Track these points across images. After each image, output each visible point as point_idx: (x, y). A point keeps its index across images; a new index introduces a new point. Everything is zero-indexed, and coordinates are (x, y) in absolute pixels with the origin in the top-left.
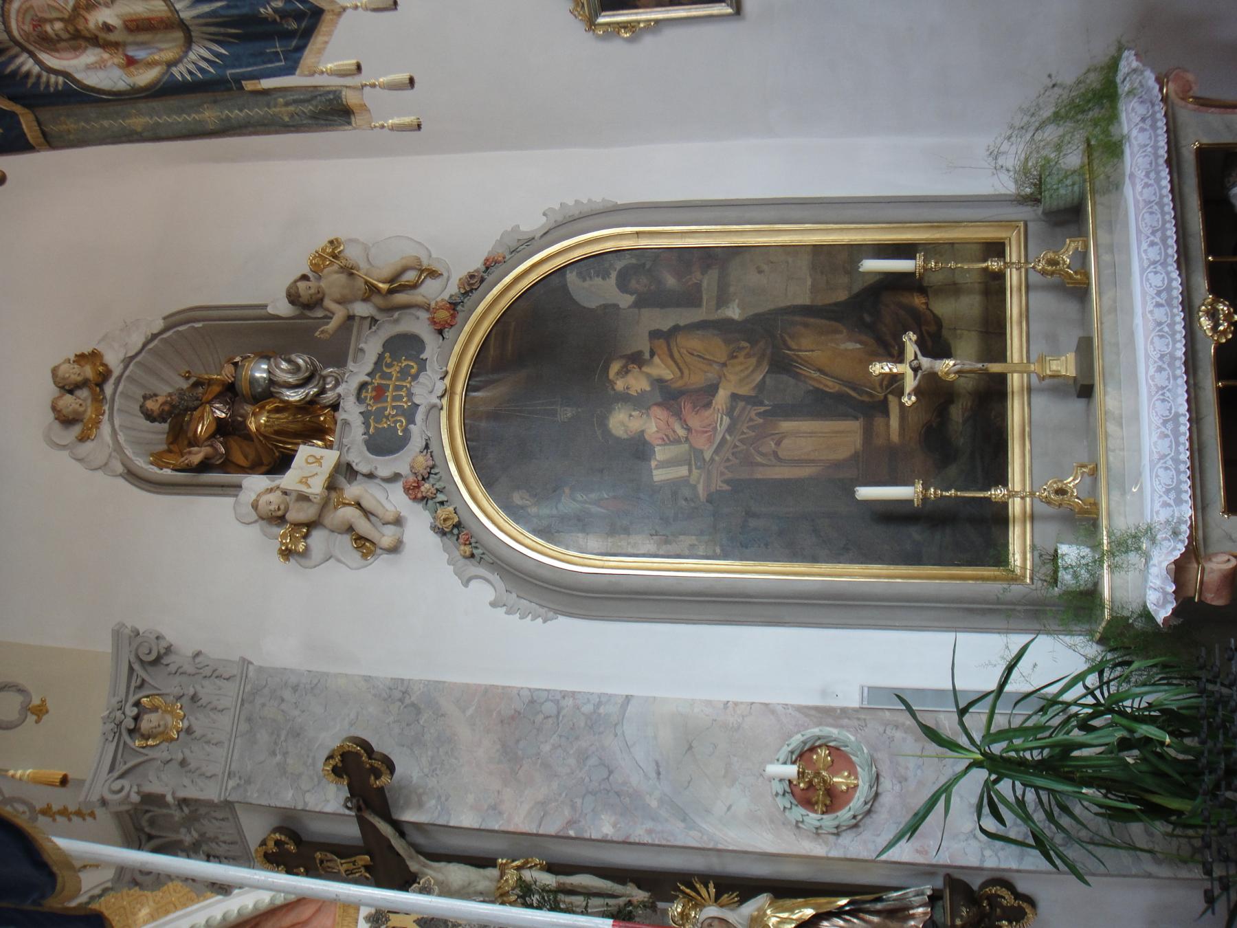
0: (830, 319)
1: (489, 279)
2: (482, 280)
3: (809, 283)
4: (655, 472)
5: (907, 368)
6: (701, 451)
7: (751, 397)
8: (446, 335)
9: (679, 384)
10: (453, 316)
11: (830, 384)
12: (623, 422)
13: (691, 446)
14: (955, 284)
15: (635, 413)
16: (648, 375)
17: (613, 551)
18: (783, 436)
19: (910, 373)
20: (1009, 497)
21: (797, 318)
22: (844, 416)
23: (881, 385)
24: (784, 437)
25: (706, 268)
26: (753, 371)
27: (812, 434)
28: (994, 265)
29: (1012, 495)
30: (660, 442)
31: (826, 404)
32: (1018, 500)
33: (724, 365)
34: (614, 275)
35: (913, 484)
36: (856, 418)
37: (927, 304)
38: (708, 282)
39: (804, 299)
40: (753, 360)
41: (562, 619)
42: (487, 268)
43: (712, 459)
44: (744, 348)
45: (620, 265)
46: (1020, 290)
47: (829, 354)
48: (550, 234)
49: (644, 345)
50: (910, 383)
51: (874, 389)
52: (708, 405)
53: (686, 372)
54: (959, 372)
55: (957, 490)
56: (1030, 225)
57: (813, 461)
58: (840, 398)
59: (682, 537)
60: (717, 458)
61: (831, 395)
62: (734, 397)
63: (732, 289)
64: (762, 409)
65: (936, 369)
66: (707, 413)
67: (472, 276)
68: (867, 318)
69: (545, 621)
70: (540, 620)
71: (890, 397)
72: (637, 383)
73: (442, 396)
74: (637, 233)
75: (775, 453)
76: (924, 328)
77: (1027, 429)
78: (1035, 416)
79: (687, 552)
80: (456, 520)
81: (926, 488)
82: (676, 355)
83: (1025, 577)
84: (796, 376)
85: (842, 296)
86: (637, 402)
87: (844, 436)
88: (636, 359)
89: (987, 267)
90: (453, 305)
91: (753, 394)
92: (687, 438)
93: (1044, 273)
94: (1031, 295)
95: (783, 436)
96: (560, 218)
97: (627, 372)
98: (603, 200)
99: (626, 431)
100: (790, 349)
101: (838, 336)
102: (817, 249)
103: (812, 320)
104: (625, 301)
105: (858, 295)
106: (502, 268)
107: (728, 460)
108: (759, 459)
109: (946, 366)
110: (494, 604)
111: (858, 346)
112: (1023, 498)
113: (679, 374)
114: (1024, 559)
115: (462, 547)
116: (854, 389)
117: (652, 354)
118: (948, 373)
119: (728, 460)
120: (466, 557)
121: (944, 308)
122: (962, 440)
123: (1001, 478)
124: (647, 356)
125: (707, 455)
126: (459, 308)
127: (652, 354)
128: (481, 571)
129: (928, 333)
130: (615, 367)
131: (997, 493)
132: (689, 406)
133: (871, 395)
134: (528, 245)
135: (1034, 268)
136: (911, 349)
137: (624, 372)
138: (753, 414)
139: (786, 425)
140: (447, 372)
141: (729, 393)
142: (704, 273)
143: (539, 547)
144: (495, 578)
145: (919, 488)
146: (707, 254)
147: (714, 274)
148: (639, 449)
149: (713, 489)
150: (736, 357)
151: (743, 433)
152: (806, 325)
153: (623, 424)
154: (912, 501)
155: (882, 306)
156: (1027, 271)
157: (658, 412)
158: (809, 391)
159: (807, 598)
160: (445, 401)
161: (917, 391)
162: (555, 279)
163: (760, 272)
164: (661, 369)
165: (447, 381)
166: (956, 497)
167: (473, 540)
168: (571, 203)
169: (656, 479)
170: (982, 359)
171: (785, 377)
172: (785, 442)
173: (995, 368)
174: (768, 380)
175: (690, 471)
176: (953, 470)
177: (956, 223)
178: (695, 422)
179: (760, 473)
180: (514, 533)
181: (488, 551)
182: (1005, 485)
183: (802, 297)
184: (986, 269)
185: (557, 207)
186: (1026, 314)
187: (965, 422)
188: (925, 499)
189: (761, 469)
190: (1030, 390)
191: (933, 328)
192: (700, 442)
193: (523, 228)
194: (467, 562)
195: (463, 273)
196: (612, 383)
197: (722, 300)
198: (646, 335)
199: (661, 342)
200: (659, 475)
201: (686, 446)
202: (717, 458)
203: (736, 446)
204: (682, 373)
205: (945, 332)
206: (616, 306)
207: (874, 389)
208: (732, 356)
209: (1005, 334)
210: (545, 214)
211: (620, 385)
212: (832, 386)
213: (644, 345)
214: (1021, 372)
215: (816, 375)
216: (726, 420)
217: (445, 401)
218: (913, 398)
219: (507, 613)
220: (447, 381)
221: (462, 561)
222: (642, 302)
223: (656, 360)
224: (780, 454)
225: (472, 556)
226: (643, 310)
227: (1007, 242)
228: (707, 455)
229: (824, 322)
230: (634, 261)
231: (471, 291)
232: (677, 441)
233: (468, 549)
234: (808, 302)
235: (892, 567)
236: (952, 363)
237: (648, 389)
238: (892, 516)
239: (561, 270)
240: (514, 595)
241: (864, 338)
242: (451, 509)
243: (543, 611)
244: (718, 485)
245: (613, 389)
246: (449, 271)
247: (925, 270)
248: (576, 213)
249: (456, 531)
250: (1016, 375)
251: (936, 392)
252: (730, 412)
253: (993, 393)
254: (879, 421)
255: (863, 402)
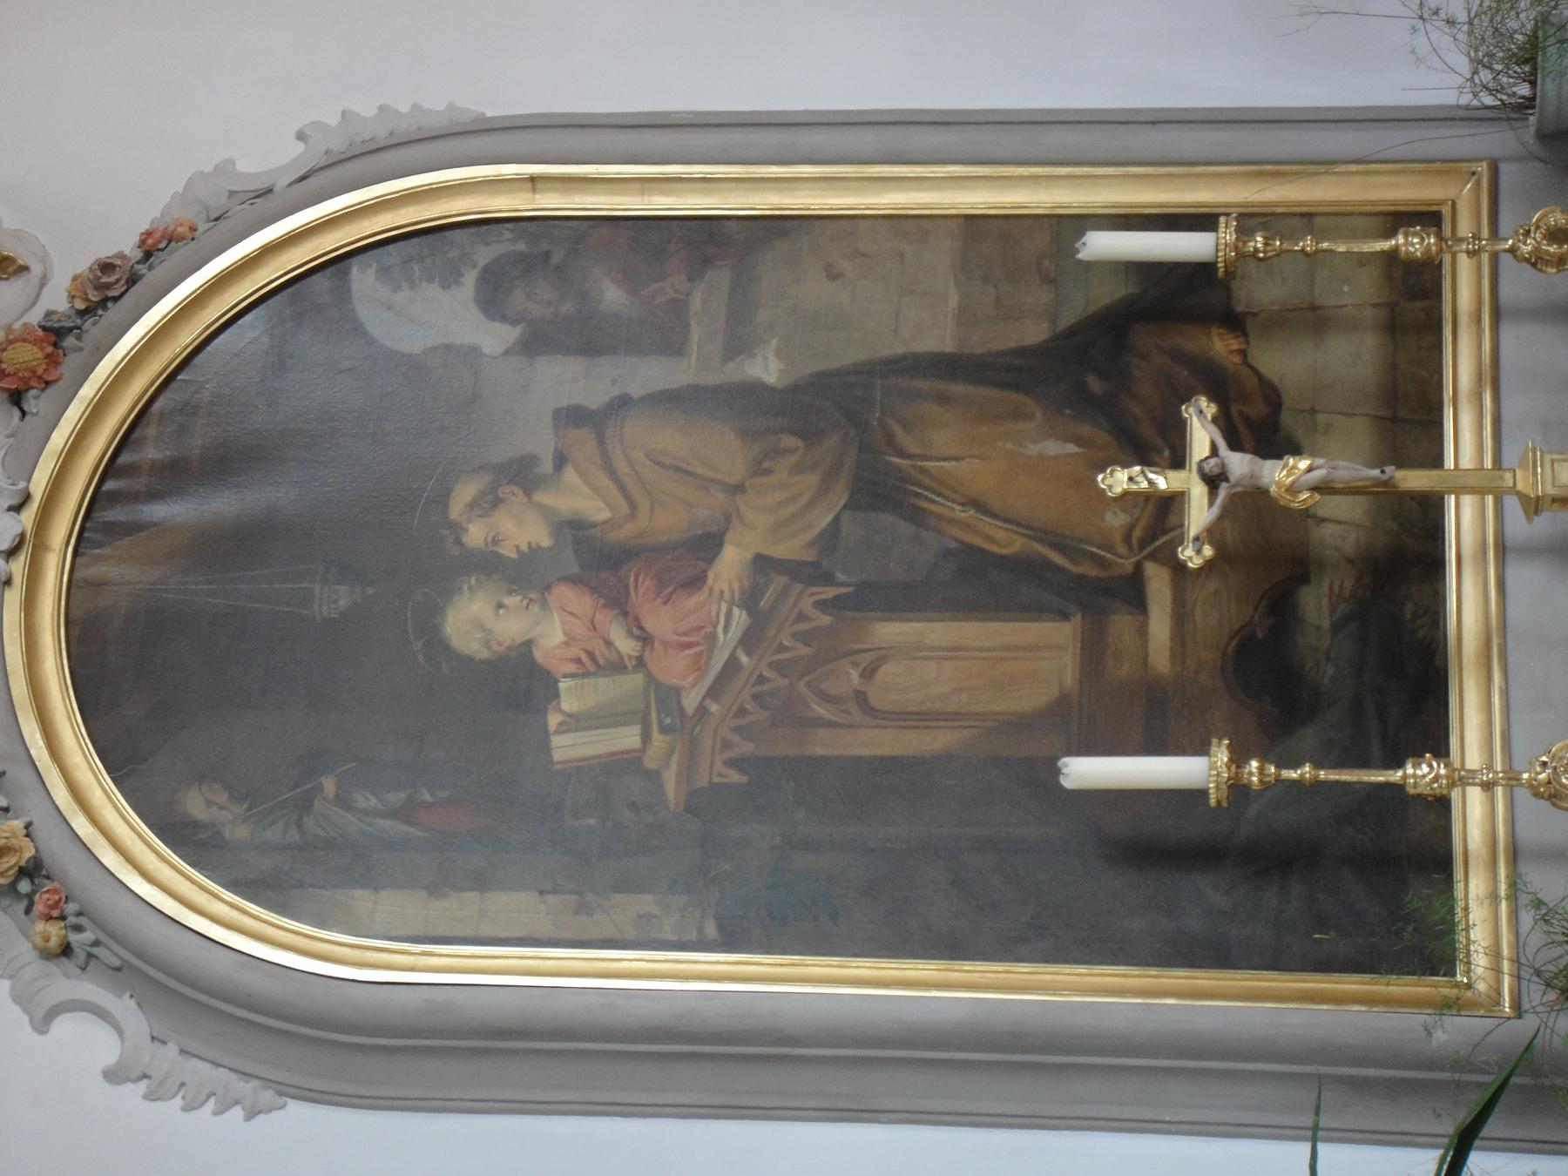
0: (1002, 385)
1: (151, 277)
2: (133, 280)
3: (953, 302)
4: (556, 741)
5: (1198, 476)
6: (677, 692)
7: (799, 564)
8: (30, 404)
9: (626, 532)
10: (53, 361)
11: (1001, 535)
12: (478, 621)
13: (650, 678)
14: (1314, 308)
15: (512, 601)
16: (547, 513)
17: (440, 932)
18: (884, 655)
19: (1198, 491)
20: (1452, 785)
21: (924, 384)
22: (1034, 611)
23: (1127, 538)
24: (883, 660)
25: (700, 265)
26: (809, 505)
27: (953, 651)
28: (1412, 244)
29: (1462, 779)
30: (572, 668)
31: (988, 583)
32: (1475, 795)
33: (738, 489)
34: (470, 278)
35: (1202, 749)
36: (1065, 616)
37: (1243, 353)
38: (707, 300)
39: (939, 338)
40: (812, 479)
41: (295, 1108)
42: (148, 255)
43: (702, 710)
44: (792, 451)
45: (485, 255)
46: (1479, 320)
47: (1002, 469)
48: (313, 181)
49: (541, 442)
50: (1200, 513)
51: (1109, 548)
52: (696, 582)
53: (644, 507)
54: (1321, 488)
55: (1318, 765)
56: (1505, 168)
57: (955, 716)
58: (1027, 568)
59: (619, 897)
60: (714, 707)
61: (1003, 562)
62: (762, 564)
63: (763, 316)
64: (831, 592)
65: (1265, 481)
66: (692, 601)
67: (106, 267)
68: (1095, 385)
69: (250, 1116)
70: (237, 1113)
71: (1151, 568)
72: (520, 529)
73: (11, 553)
74: (533, 179)
75: (861, 698)
76: (1234, 409)
77: (1495, 641)
78: (1515, 612)
79: (630, 934)
80: (29, 853)
81: (1238, 759)
82: (621, 466)
83: (1498, 1002)
84: (917, 516)
85: (1034, 333)
86: (521, 575)
87: (1037, 655)
88: (521, 475)
89: (1394, 252)
90: (55, 334)
91: (809, 556)
92: (640, 662)
93: (1536, 261)
94: (1508, 333)
95: (884, 655)
96: (338, 145)
97: (497, 503)
98: (451, 107)
99: (487, 644)
100: (902, 454)
101: (1020, 425)
102: (973, 224)
103: (958, 389)
104: (494, 338)
105: (1071, 333)
106: (181, 253)
107: (742, 712)
108: (819, 710)
109: (1284, 475)
110: (113, 1076)
111: (1072, 448)
112: (1488, 787)
113: (625, 509)
114: (1497, 970)
115: (40, 926)
116: (1060, 548)
117: (560, 461)
118: (1293, 489)
119: (742, 712)
120: (46, 955)
121: (1284, 363)
122: (1331, 670)
123: (1435, 742)
124: (547, 466)
125: (690, 701)
126: (70, 341)
127: (560, 461)
128: (88, 989)
129: (1247, 420)
130: (465, 492)
131: (1420, 774)
132: (647, 584)
133: (1101, 563)
134: (264, 201)
135: (1512, 250)
136: (1201, 436)
137: (489, 502)
138: (807, 604)
139: (891, 631)
140: (27, 498)
141: (749, 555)
142: (695, 274)
143: (248, 922)
144: (124, 1007)
145: (1221, 755)
146: (705, 239)
147: (721, 276)
148: (520, 683)
149: (702, 781)
150: (769, 472)
151: (782, 648)
152: (943, 399)
153: (479, 625)
154: (1202, 793)
155: (1135, 346)
156: (1495, 258)
157: (566, 594)
158: (947, 553)
159: (932, 1046)
160: (18, 567)
161: (1212, 533)
162: (320, 282)
163: (833, 276)
164: (581, 497)
165: (28, 517)
166: (1317, 785)
167: (71, 908)
168: (369, 112)
169: (558, 756)
170: (1380, 463)
171: (888, 519)
172: (888, 671)
173: (1414, 480)
174: (846, 519)
175: (646, 738)
176: (1308, 736)
177: (1324, 165)
178: (661, 620)
179: (823, 745)
180: (184, 887)
181: (112, 934)
182: (1441, 752)
183: (935, 333)
184: (1392, 256)
185: (333, 120)
186: (1493, 376)
187: (1336, 628)
188: (1238, 789)
189: (821, 732)
190: (1502, 549)
191: (1258, 409)
192: (672, 667)
193: (243, 166)
194: (51, 967)
195: (83, 263)
196: (457, 529)
197: (738, 345)
198: (547, 419)
199: (583, 444)
200: (566, 747)
201: (638, 679)
202: (714, 707)
203: (762, 679)
204: (633, 506)
205: (1287, 419)
206: (474, 350)
207: (1109, 548)
208: (759, 470)
209: (1439, 424)
210: (301, 136)
211: (476, 535)
212: (1006, 542)
213: (541, 442)
214: (1480, 492)
215: (968, 514)
216: (740, 618)
217: (18, 567)
218: (1208, 551)
219: (150, 1097)
220: (28, 517)
221: (37, 967)
222: (535, 343)
223: (570, 475)
224: (873, 700)
225: (66, 950)
226: (542, 362)
227: (1446, 211)
228: (690, 701)
229: (994, 393)
230: (521, 246)
231: (103, 303)
232: (617, 667)
233: (55, 931)
234: (949, 347)
235: (1153, 971)
236: (1304, 464)
237: (546, 542)
238: (1153, 841)
239: (338, 262)
240: (172, 1049)
241: (1086, 429)
242: (17, 824)
243: (246, 1088)
244: (715, 770)
245: (458, 542)
246: (45, 259)
247: (1241, 255)
248: (382, 134)
249: (24, 886)
250: (1468, 501)
251: (1266, 548)
252: (750, 600)
253: (1407, 553)
254: (1121, 624)
255: (1081, 578)
